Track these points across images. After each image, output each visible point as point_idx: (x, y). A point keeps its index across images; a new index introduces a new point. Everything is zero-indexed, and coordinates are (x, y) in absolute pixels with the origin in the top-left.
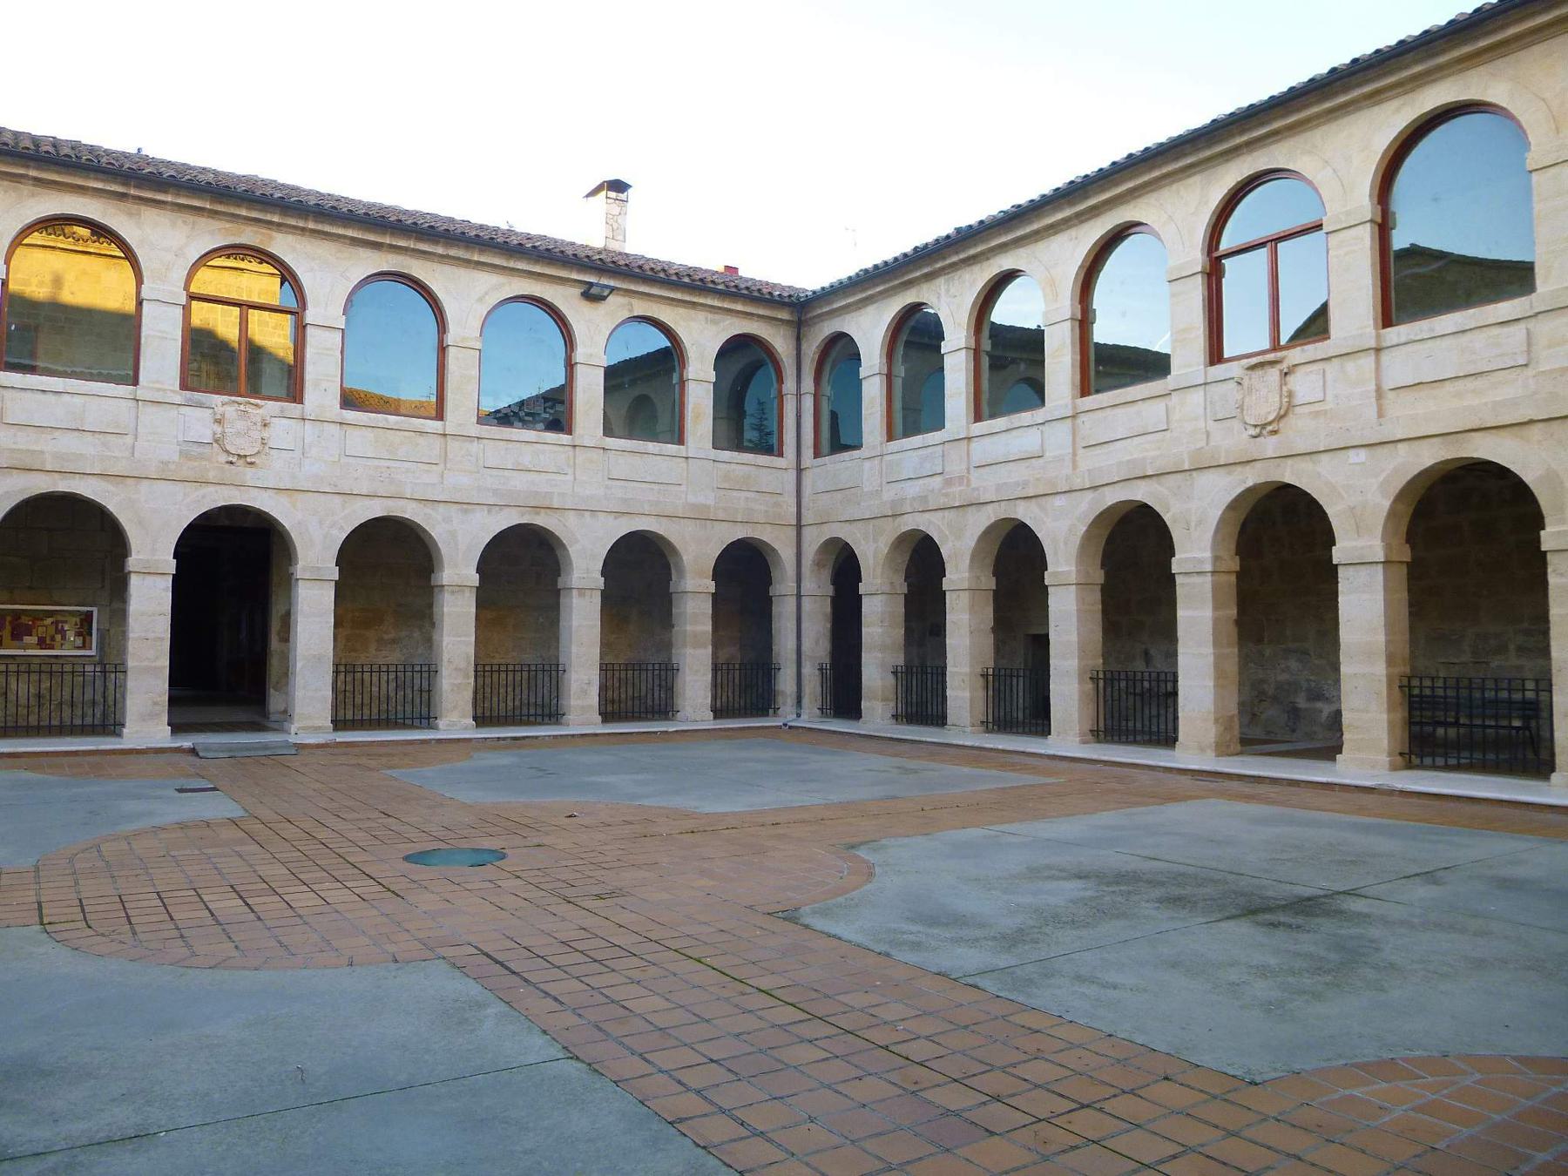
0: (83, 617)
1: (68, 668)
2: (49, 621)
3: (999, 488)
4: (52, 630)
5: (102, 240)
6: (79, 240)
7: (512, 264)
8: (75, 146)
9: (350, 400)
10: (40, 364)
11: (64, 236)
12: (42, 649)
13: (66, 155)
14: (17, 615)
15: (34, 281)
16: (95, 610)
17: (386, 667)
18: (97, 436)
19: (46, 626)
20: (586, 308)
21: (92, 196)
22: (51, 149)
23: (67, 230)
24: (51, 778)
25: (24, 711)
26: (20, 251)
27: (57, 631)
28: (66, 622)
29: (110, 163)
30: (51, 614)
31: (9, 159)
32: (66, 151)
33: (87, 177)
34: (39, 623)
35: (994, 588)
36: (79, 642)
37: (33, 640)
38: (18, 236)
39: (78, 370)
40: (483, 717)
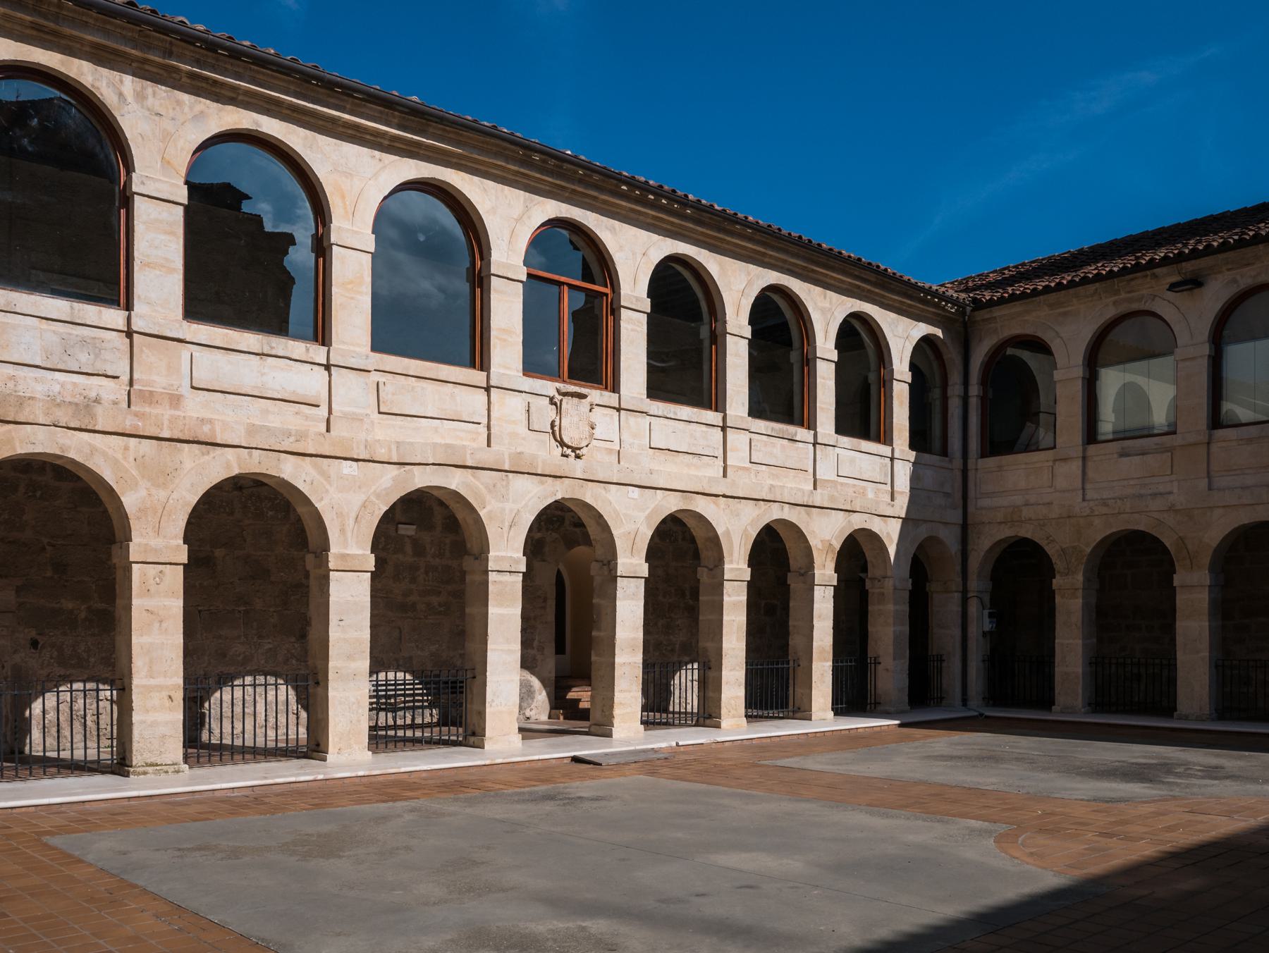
3: (252, 430)
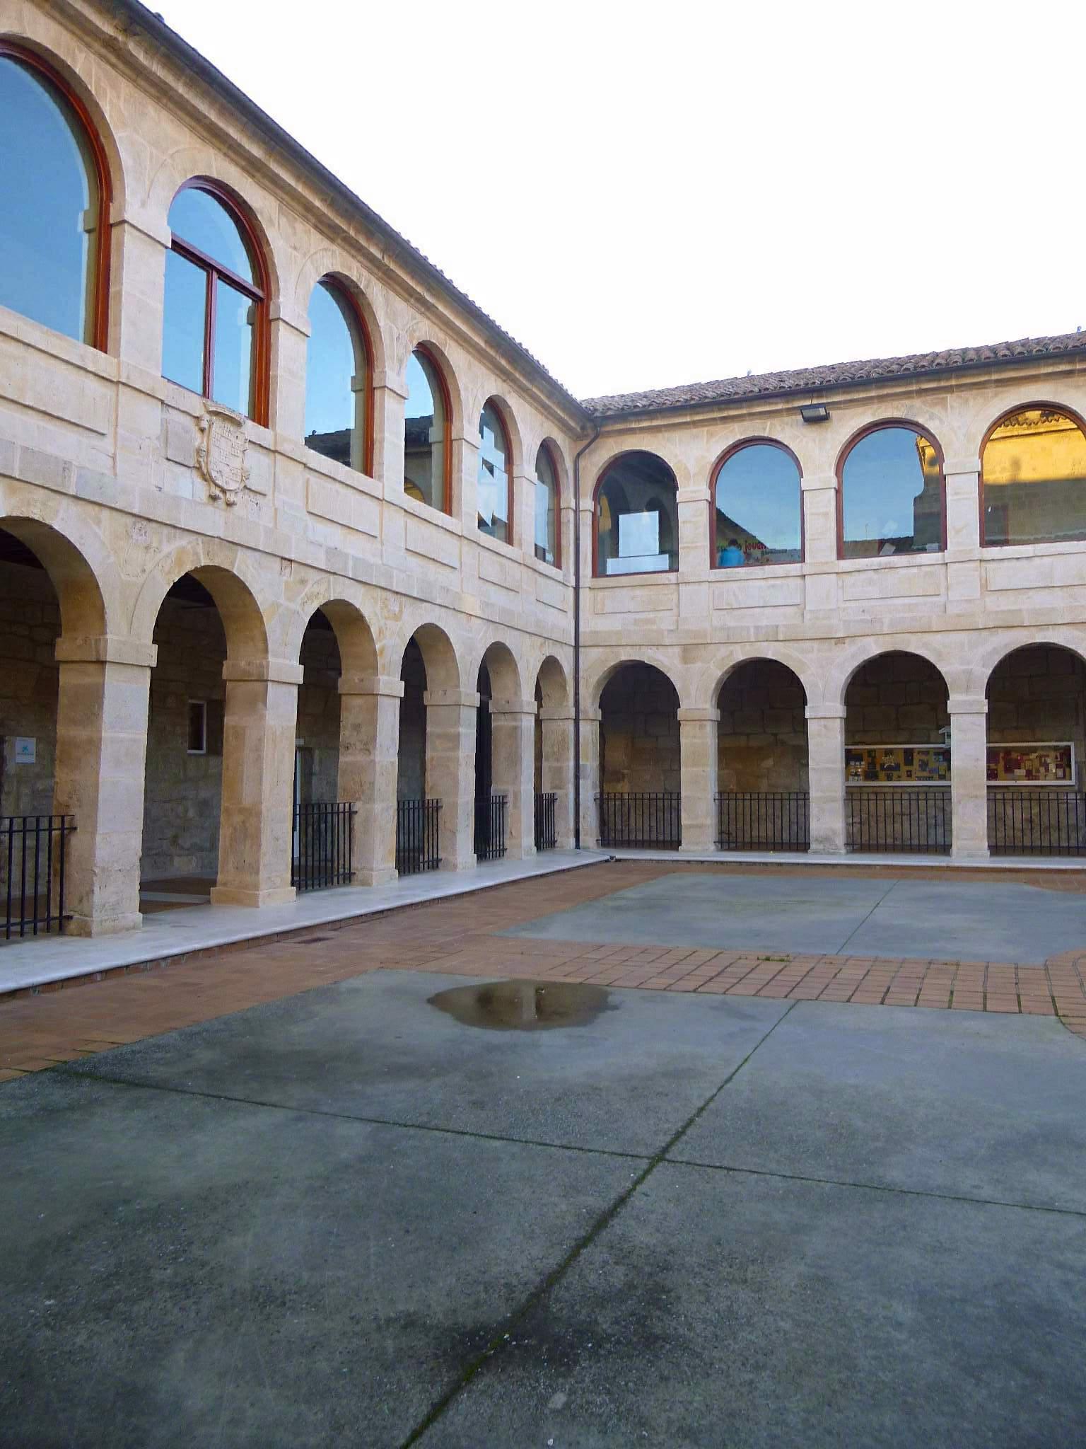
0: (1062, 751)
1: (1052, 796)
2: (1033, 756)
4: (1037, 763)
5: (1056, 417)
6: (1030, 424)
7: (655, 423)
8: (1025, 343)
9: (845, 549)
10: (1010, 538)
11: (1019, 424)
12: (1029, 780)
13: (1020, 353)
14: (1008, 751)
15: (998, 468)
16: (1072, 744)
17: (924, 795)
18: (1065, 589)
19: (1031, 760)
20: (812, 432)
21: (1044, 380)
22: (1007, 352)
23: (1020, 418)
24: (1048, 892)
25: (1019, 834)
26: (989, 445)
27: (1041, 764)
28: (1048, 756)
29: (1057, 348)
30: (1034, 750)
31: (975, 372)
32: (1019, 349)
33: (1039, 366)
34: (1025, 757)
35: (302, 682)
36: (1060, 773)
37: (1022, 772)
38: (719, 461)
39: (1039, 536)
40: (782, 843)
